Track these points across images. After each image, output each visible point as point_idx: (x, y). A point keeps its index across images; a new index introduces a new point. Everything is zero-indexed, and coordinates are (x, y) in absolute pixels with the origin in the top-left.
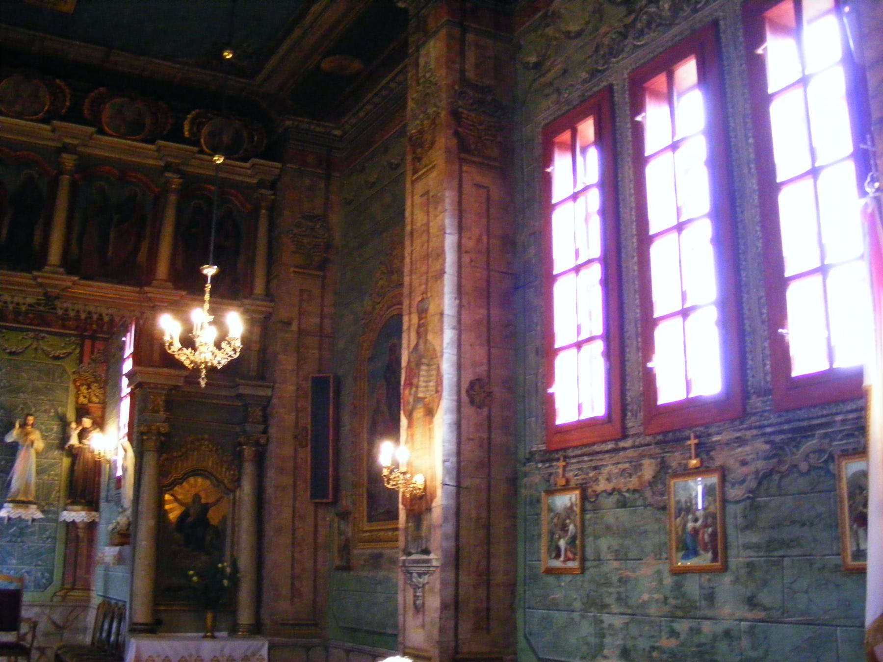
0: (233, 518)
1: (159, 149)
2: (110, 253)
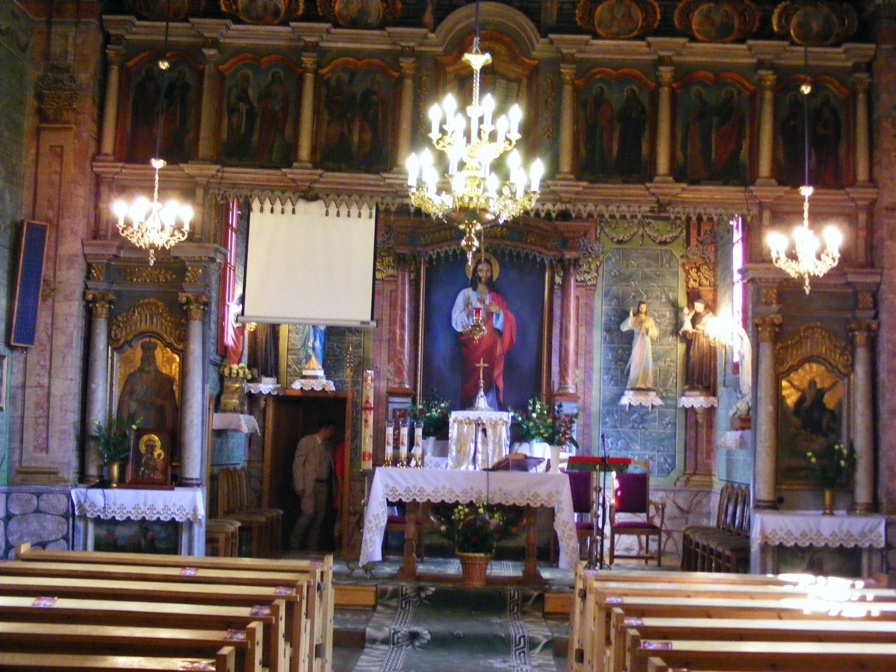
0: (849, 402)
1: (750, 48)
2: (713, 156)
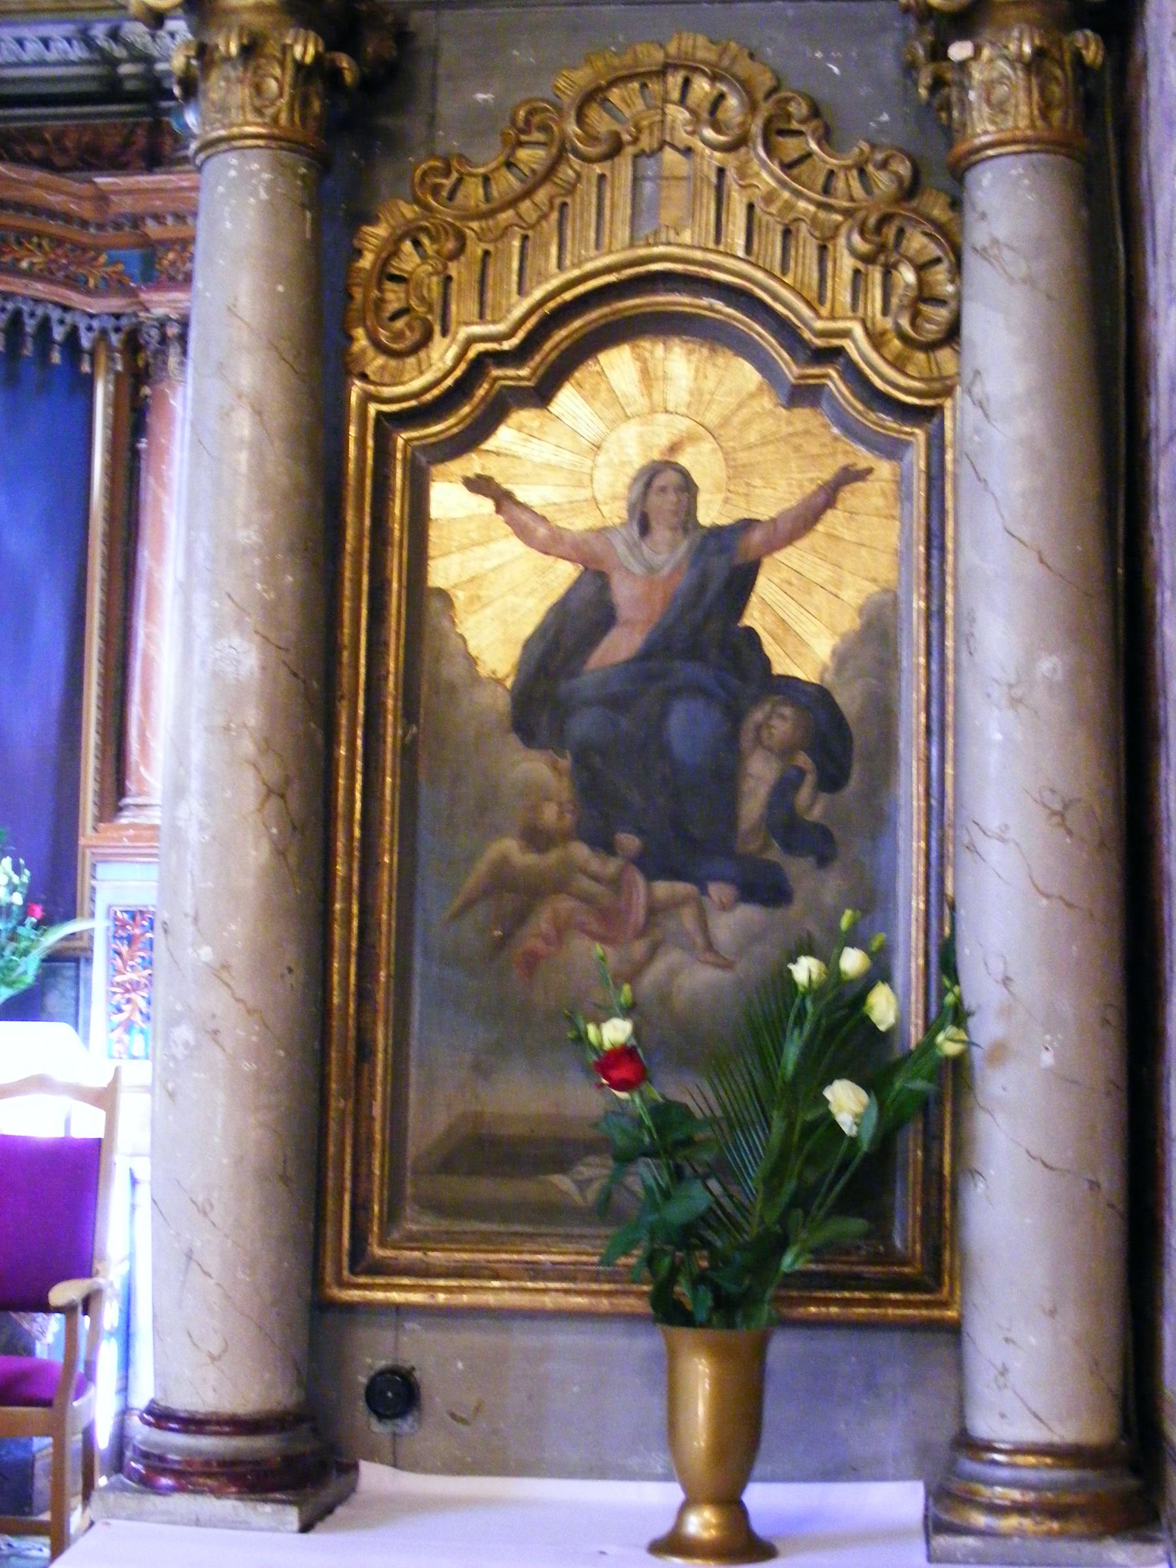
0: (935, 615)
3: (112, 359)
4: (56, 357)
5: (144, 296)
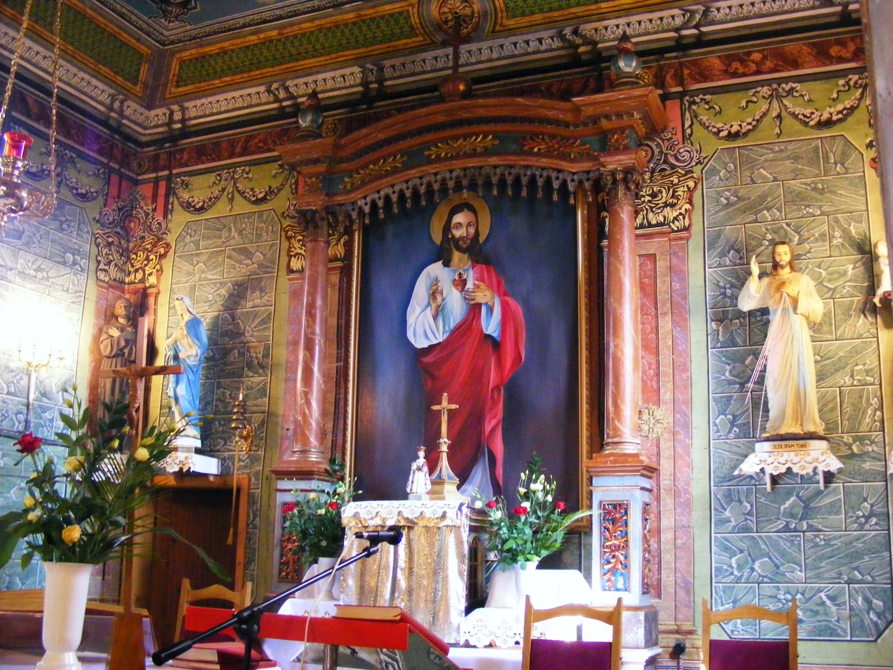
3: (586, 196)
4: (555, 197)
5: (602, 160)
